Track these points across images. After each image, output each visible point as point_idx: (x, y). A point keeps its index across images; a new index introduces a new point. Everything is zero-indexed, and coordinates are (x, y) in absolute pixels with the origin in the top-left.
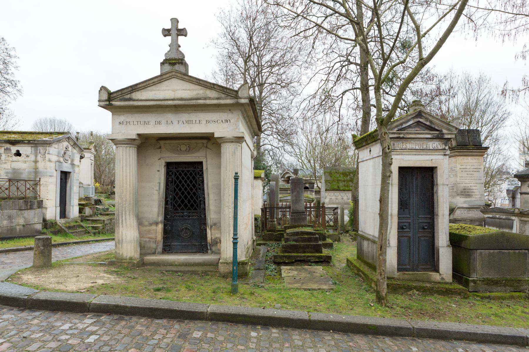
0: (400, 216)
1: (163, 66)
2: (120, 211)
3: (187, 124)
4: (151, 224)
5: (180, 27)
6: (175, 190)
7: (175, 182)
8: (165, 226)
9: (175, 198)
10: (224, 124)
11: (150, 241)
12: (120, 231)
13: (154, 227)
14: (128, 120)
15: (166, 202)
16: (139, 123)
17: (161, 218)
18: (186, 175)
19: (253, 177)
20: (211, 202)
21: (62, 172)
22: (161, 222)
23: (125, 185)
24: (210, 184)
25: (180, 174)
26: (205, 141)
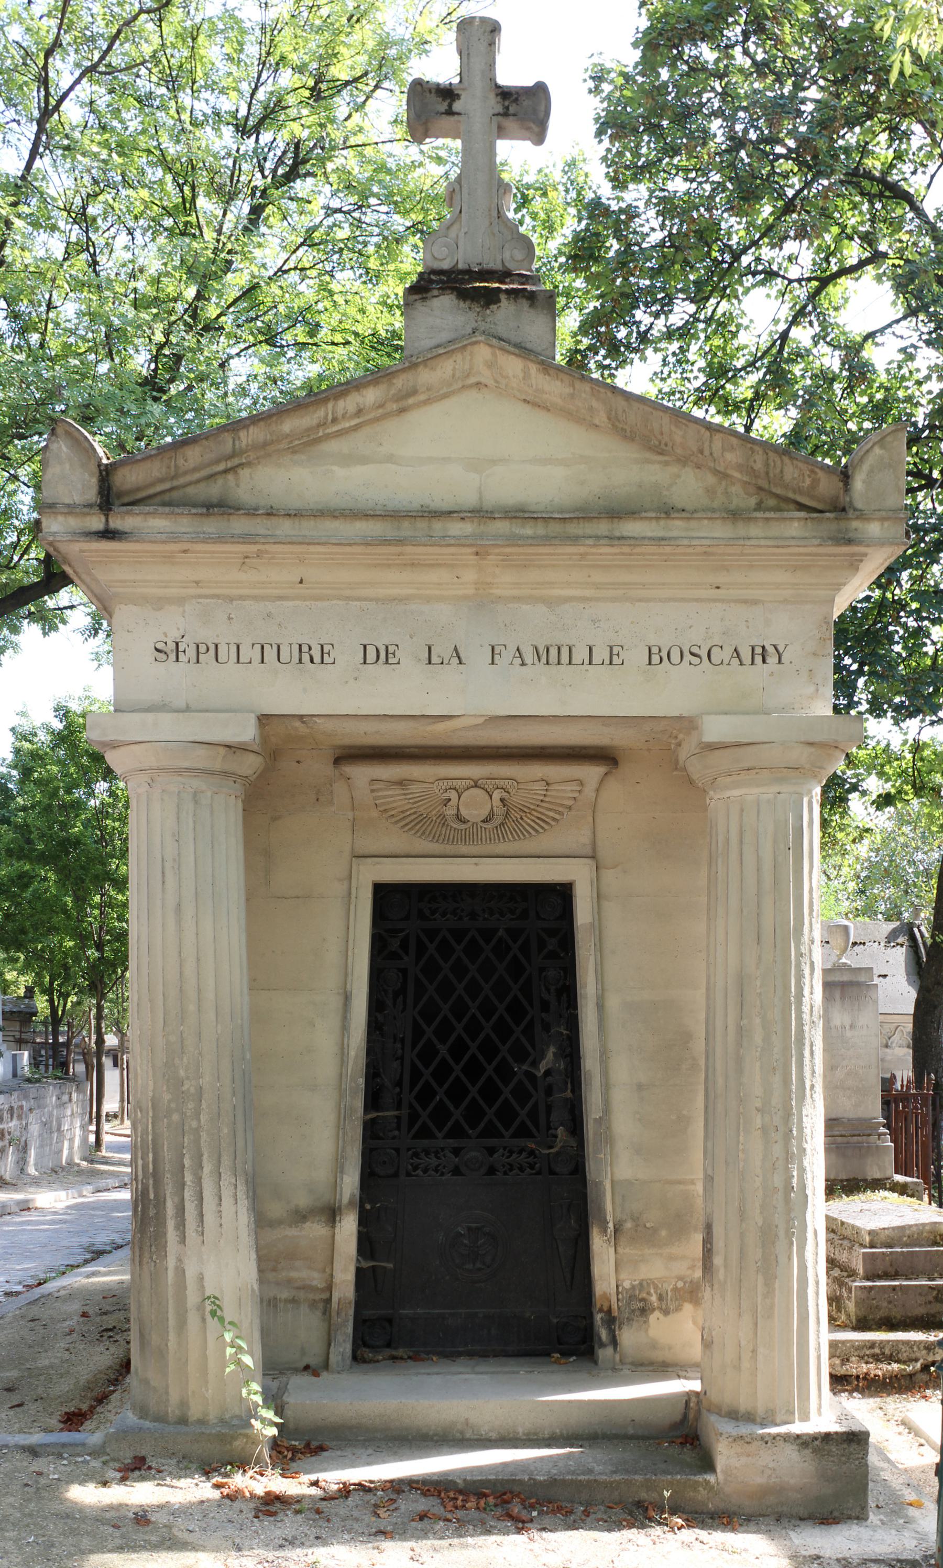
1: (421, 308)
2: (167, 1154)
3: (541, 666)
4: (300, 1217)
5: (512, 71)
6: (418, 1033)
9: (416, 1074)
10: (747, 668)
11: (294, 1301)
12: (171, 1262)
14: (207, 635)
15: (373, 1099)
16: (270, 654)
17: (350, 1183)
21: (465, 26)
23: (192, 1008)
26: (592, 773)
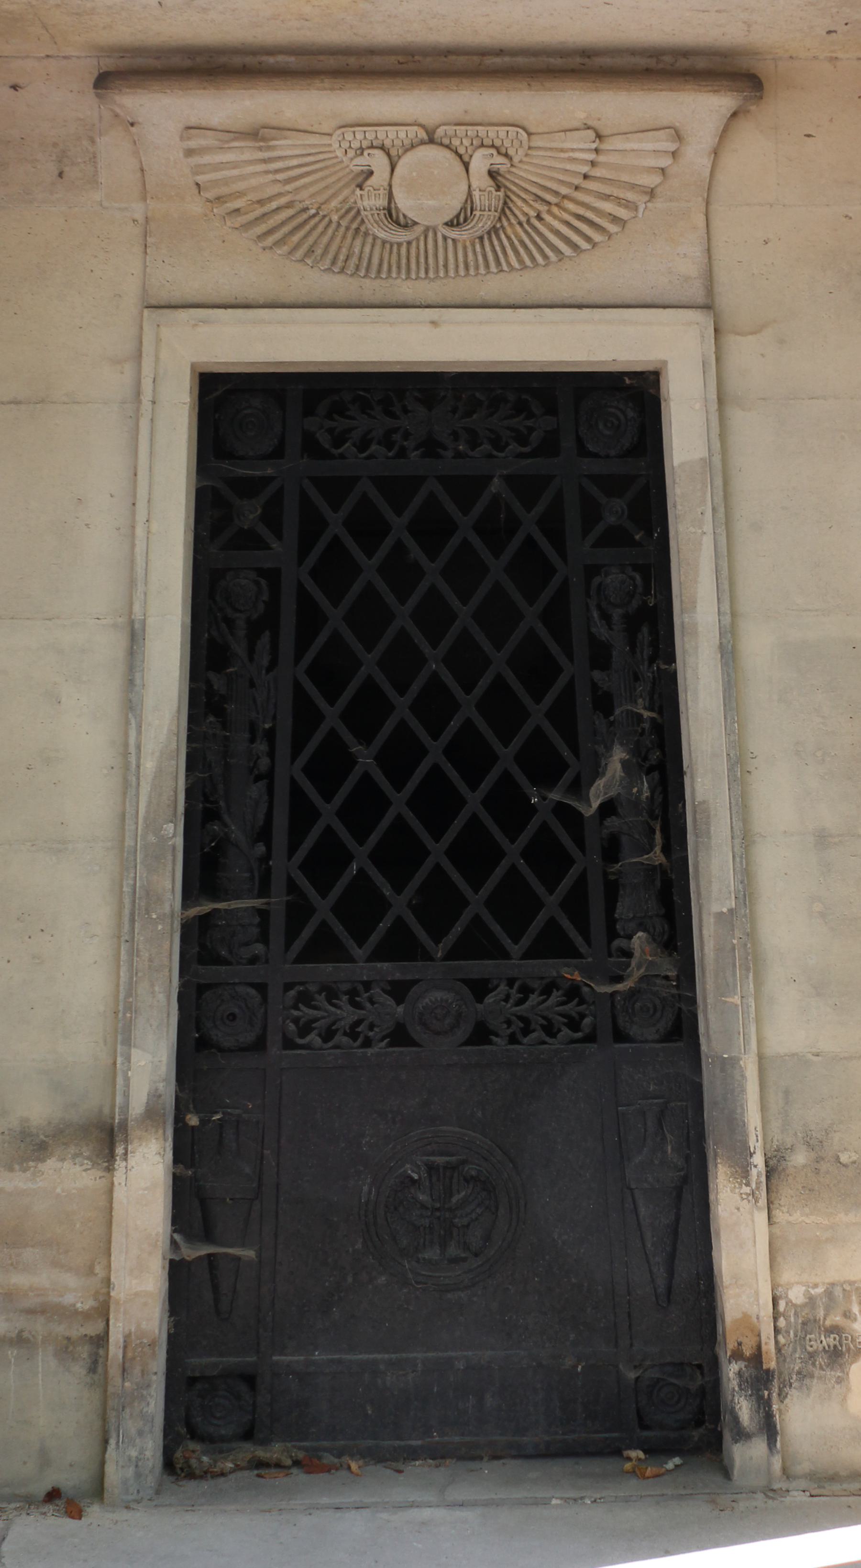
0: (199, 1362)
6: (306, 716)
7: (310, 619)
8: (186, 1150)
13: (69, 1176)
15: (204, 870)
17: (150, 1066)
18: (432, 530)
19: (91, 93)
20: (779, 865)
22: (151, 1114)
24: (758, 645)
25: (368, 529)
